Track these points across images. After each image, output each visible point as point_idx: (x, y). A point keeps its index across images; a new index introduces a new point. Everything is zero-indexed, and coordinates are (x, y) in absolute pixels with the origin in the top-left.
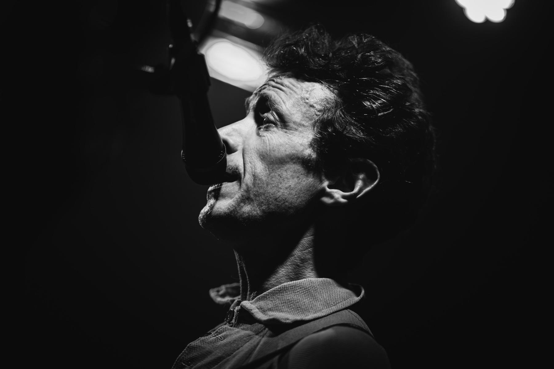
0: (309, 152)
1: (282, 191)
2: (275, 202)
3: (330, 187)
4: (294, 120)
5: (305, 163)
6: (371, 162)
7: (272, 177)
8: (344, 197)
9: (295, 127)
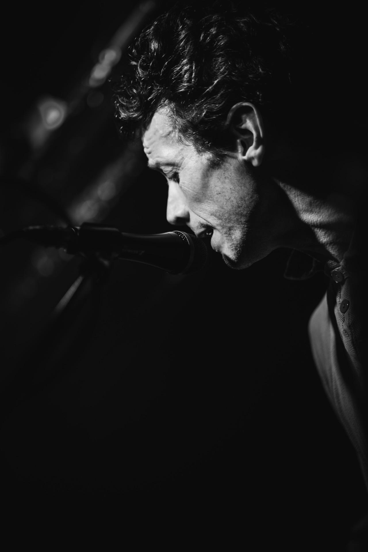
0: (208, 155)
1: (232, 199)
2: (241, 209)
3: (244, 154)
4: (174, 156)
5: (214, 165)
6: (234, 106)
7: (217, 201)
8: (256, 148)
9: (180, 157)
